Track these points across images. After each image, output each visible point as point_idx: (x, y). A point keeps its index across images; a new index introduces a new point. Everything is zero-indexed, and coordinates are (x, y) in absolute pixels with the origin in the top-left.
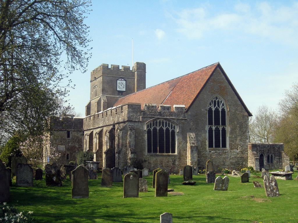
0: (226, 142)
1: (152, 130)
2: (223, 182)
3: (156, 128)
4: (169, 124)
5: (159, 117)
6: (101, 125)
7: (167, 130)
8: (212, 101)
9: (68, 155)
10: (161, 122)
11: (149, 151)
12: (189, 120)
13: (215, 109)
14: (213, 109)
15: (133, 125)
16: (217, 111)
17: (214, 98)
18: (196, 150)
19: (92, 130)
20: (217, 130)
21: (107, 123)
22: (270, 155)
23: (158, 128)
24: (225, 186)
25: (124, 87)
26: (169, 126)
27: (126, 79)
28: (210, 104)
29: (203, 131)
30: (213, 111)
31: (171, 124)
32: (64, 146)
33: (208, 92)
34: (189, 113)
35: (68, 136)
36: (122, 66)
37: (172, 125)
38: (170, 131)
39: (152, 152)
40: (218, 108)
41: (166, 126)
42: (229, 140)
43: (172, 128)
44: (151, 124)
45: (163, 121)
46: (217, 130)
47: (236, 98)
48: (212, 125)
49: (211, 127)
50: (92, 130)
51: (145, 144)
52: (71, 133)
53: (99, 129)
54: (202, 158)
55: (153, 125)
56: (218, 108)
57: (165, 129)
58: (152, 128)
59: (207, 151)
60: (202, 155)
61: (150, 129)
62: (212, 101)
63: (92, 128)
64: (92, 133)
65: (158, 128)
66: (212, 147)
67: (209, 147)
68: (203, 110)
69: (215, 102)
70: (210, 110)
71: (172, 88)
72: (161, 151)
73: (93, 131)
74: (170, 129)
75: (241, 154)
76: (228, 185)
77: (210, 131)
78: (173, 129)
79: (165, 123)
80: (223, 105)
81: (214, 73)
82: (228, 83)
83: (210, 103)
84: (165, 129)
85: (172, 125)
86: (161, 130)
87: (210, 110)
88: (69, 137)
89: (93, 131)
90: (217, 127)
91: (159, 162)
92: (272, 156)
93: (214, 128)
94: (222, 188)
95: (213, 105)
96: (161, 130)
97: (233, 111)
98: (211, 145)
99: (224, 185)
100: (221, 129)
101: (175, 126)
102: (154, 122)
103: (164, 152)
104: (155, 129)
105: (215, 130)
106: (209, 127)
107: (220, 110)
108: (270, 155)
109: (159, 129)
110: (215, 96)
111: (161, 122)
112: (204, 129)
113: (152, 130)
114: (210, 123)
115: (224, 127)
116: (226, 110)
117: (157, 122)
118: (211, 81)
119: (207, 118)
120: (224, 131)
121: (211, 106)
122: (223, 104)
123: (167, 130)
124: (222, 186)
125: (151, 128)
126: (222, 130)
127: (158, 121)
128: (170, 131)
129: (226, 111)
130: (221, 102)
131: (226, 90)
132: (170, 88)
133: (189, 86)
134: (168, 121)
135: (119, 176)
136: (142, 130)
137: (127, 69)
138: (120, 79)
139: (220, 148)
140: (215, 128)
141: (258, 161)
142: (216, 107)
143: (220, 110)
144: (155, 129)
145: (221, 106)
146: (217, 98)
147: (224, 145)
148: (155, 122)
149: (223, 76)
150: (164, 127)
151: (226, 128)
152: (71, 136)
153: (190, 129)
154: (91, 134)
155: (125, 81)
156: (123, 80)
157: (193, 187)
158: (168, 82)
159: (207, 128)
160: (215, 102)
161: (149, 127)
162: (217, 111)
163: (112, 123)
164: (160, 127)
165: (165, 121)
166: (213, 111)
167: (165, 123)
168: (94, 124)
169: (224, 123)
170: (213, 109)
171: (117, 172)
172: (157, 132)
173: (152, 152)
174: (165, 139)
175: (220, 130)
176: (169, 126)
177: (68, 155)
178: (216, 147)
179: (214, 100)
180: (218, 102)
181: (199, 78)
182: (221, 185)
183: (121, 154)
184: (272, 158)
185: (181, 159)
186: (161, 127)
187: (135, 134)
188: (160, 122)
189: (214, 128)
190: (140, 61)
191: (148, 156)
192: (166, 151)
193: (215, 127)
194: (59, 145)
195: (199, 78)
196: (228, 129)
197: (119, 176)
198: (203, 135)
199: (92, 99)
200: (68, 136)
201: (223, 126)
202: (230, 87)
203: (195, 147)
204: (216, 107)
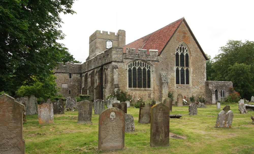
0: (189, 81)
1: (132, 69)
2: (227, 118)
3: (136, 68)
4: (146, 64)
5: (137, 58)
6: (93, 68)
7: (144, 69)
8: (179, 48)
9: (70, 91)
10: (140, 62)
11: (130, 86)
12: (161, 62)
13: (181, 54)
14: (180, 54)
15: (117, 65)
16: (182, 55)
17: (180, 46)
18: (167, 86)
19: (87, 73)
20: (182, 70)
21: (97, 65)
22: (223, 91)
23: (137, 68)
24: (228, 123)
26: (146, 66)
27: (112, 41)
28: (177, 50)
29: (172, 71)
30: (180, 55)
31: (147, 64)
32: (67, 85)
33: (175, 40)
34: (161, 56)
35: (70, 77)
36: (110, 32)
37: (148, 66)
38: (147, 70)
39: (132, 87)
40: (183, 53)
41: (143, 66)
42: (192, 78)
43: (148, 68)
44: (131, 64)
45: (141, 62)
46: (182, 70)
47: (196, 46)
48: (179, 66)
49: (177, 68)
50: (87, 73)
51: (127, 80)
52: (72, 75)
53: (91, 71)
55: (133, 65)
56: (183, 53)
57: (142, 68)
58: (132, 68)
60: (172, 90)
62: (179, 48)
63: (87, 70)
64: (87, 74)
65: (137, 68)
66: (179, 83)
67: (177, 83)
68: (171, 54)
69: (181, 48)
70: (177, 55)
71: (146, 41)
72: (140, 86)
73: (87, 73)
74: (146, 68)
75: (201, 89)
76: (232, 122)
77: (177, 71)
79: (142, 64)
80: (187, 51)
81: (180, 26)
82: (190, 34)
83: (177, 49)
84: (142, 68)
85: (148, 66)
86: (140, 69)
87: (177, 55)
88: (71, 78)
89: (87, 73)
90: (182, 68)
91: (138, 96)
92: (224, 91)
93: (180, 69)
94: (225, 125)
95: (179, 50)
96: (140, 69)
97: (195, 56)
98: (178, 82)
99: (227, 122)
100: (185, 69)
101: (150, 66)
102: (133, 62)
103: (146, 88)
104: (134, 69)
105: (181, 71)
106: (176, 68)
107: (185, 54)
108: (223, 91)
109: (138, 69)
110: (181, 43)
111: (140, 62)
112: (172, 68)
113: (132, 69)
114: (177, 65)
115: (187, 68)
116: (189, 55)
117: (136, 63)
118: (177, 32)
119: (175, 61)
120: (187, 71)
121: (178, 51)
122: (187, 50)
123: (144, 69)
124: (225, 123)
125: (131, 67)
126: (186, 71)
127: (137, 62)
128: (147, 70)
129: (189, 56)
130: (185, 48)
131: (189, 39)
132: (143, 42)
133: (159, 37)
134: (145, 62)
135: (103, 109)
136: (124, 69)
137: (113, 34)
138: (109, 41)
139: (184, 85)
140: (181, 69)
141: (214, 95)
142: (181, 52)
143: (185, 54)
144: (134, 69)
145: (185, 51)
146: (182, 45)
147: (188, 83)
148: (135, 62)
149: (187, 29)
150: (141, 67)
151: (189, 69)
152: (72, 77)
153: (162, 69)
154: (86, 75)
155: (112, 42)
156: (110, 41)
157: (178, 119)
158: (142, 38)
159: (175, 68)
160: (181, 48)
161: (129, 67)
162: (182, 55)
163: (100, 65)
164: (139, 67)
166: (180, 55)
167: (142, 64)
168: (88, 68)
169: (187, 65)
170: (180, 54)
171: (100, 105)
172: (136, 71)
173: (132, 87)
174: (142, 77)
175: (184, 71)
176: (146, 66)
177: (70, 91)
178: (181, 83)
179: (180, 47)
180: (183, 48)
181: (168, 31)
182: (224, 122)
183: (107, 89)
184: (224, 93)
185: (155, 93)
186: (140, 67)
187: (119, 72)
188: (138, 63)
189: (180, 69)
190: (122, 29)
191: (129, 91)
192: (148, 87)
193: (181, 68)
194: (63, 84)
195: (168, 31)
196: (191, 69)
197: (103, 109)
198: (172, 74)
199: (90, 54)
200: (70, 77)
201: (187, 67)
203: (166, 83)
204: (181, 52)
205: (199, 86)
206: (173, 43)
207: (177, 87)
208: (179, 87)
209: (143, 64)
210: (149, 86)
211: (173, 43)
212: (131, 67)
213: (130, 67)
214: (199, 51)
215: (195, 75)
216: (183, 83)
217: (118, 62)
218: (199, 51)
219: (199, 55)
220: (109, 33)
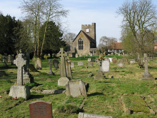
20: (81, 46)
46: (81, 46)
77: (79, 46)
98: (79, 49)
114: (79, 44)
120: (83, 46)
147: (83, 49)
159: (78, 45)
162: (81, 41)
169: (83, 44)
196: (84, 45)
216: (81, 49)
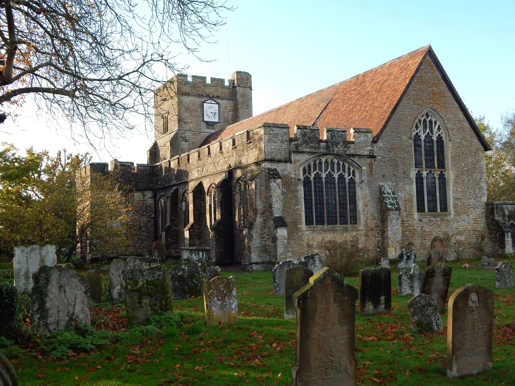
12: (380, 158)
25: (207, 111)
29: (406, 179)
34: (380, 144)
38: (347, 181)
54: (407, 233)
55: (315, 169)
59: (414, 220)
60: (407, 226)
61: (309, 176)
68: (404, 138)
69: (425, 121)
75: (475, 223)
77: (419, 179)
78: (351, 176)
95: (421, 128)
98: (421, 209)
100: (437, 176)
114: (418, 164)
120: (442, 177)
122: (439, 126)
127: (324, 160)
128: (347, 181)
137: (218, 82)
138: (209, 102)
139: (424, 213)
146: (427, 116)
147: (445, 208)
153: (384, 176)
155: (218, 104)
156: (213, 102)
165: (341, 163)
169: (442, 165)
180: (430, 121)
196: (451, 175)
202: (450, 94)
205: (471, 216)
206: (406, 110)
207: (420, 220)
208: (423, 220)
209: (338, 164)
210: (355, 220)
211: (407, 110)
212: (310, 174)
213: (318, 171)
214: (467, 128)
215: (459, 189)
217: (279, 161)
218: (467, 128)
219: (468, 138)
220: (209, 81)
